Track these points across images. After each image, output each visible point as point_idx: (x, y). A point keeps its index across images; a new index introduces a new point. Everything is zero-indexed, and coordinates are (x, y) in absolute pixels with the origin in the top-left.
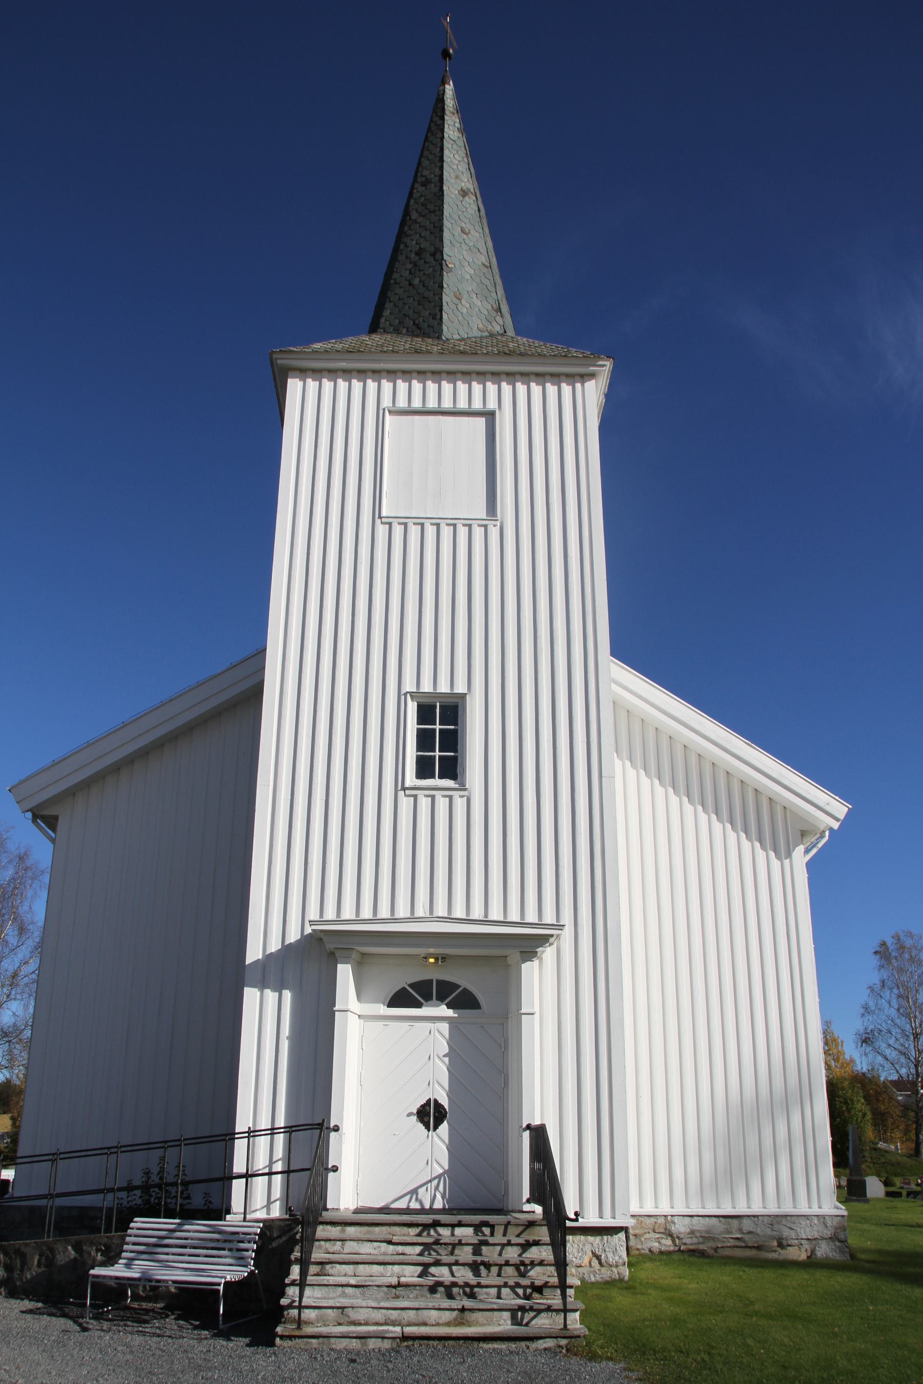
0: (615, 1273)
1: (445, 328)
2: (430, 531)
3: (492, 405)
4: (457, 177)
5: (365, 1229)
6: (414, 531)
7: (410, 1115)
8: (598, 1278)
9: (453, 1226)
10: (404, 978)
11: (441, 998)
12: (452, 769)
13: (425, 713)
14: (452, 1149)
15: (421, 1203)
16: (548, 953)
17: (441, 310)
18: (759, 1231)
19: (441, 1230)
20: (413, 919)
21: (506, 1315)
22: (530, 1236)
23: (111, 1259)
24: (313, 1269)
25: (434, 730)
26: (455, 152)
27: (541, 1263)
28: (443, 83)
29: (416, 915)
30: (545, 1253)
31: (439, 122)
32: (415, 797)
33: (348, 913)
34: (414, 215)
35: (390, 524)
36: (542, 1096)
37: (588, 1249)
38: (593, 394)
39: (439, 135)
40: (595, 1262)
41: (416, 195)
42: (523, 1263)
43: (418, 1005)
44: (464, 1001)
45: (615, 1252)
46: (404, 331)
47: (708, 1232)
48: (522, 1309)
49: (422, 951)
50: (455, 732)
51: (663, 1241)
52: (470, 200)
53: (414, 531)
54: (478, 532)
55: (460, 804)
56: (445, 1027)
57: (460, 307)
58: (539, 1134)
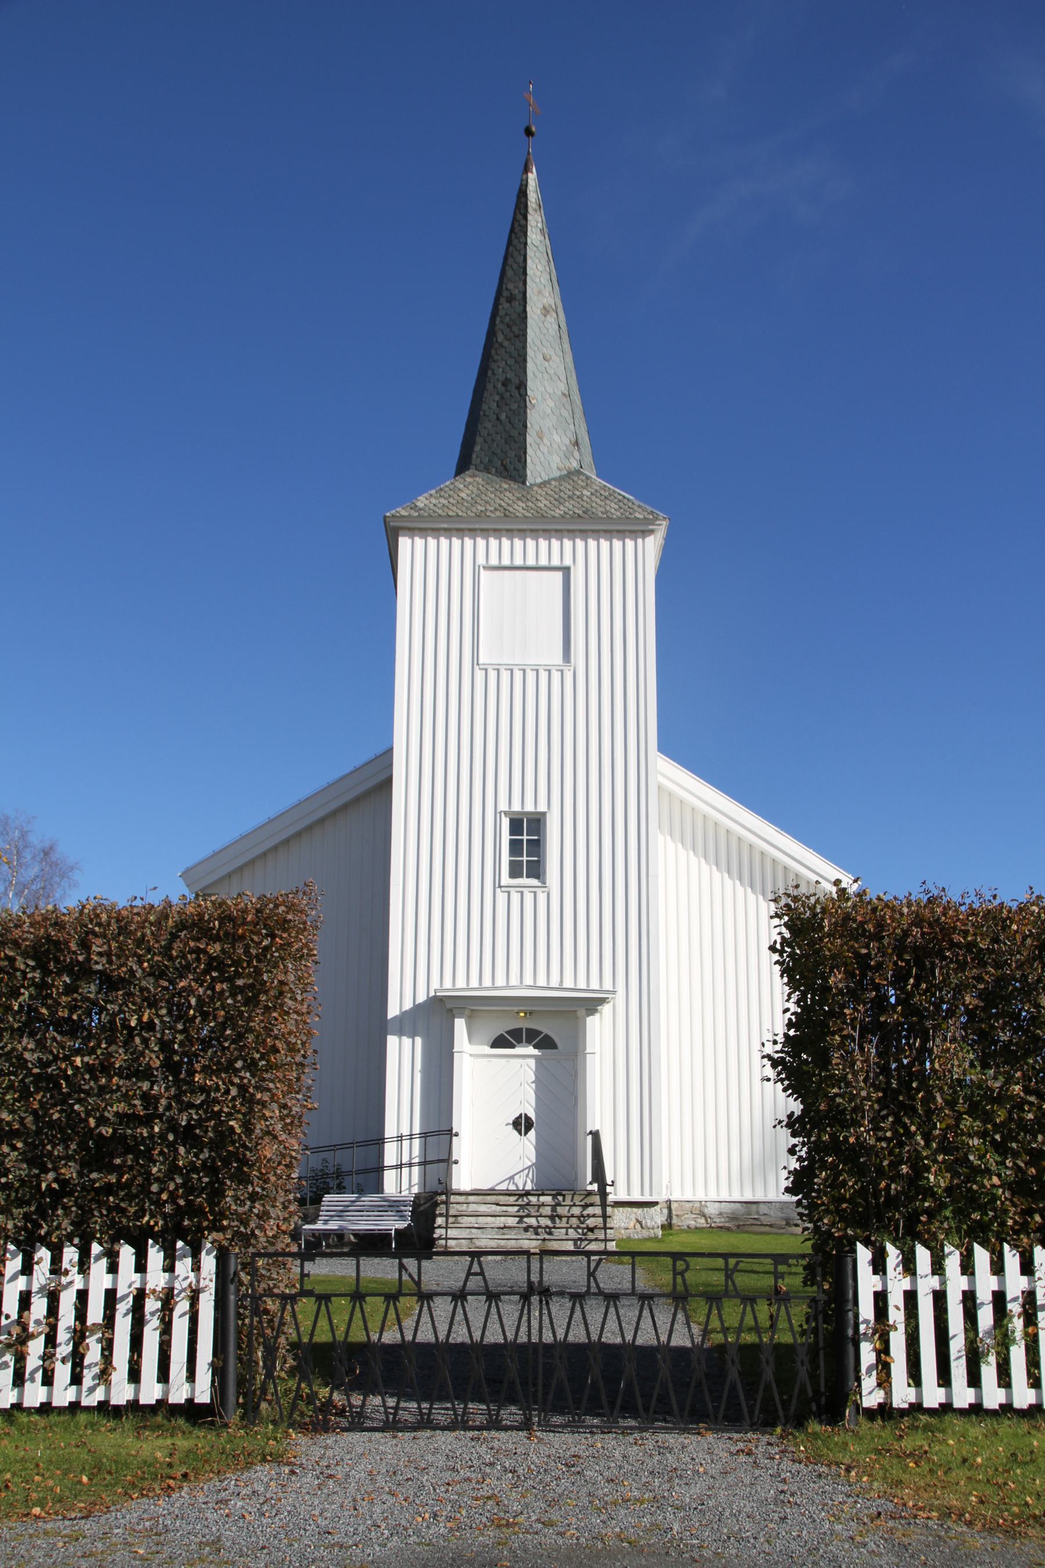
0: (652, 1233)
1: (529, 473)
2: (518, 675)
3: (568, 562)
4: (540, 292)
5: (481, 1197)
6: (505, 676)
7: (507, 1124)
8: (640, 1236)
9: (539, 1195)
10: (502, 1027)
11: (529, 1042)
12: (536, 870)
13: (516, 826)
14: (538, 1148)
15: (516, 1185)
16: (606, 1009)
17: (525, 453)
18: (772, 1213)
19: (531, 1198)
20: (508, 987)
21: (571, 1243)
22: (588, 1200)
23: (314, 1221)
24: (451, 1220)
25: (522, 840)
26: (537, 261)
27: (594, 1216)
28: (526, 170)
29: (511, 984)
30: (598, 1211)
31: (523, 222)
32: (509, 893)
33: (461, 983)
34: (500, 338)
35: (486, 670)
36: (601, 1109)
37: (633, 1217)
38: (651, 548)
39: (522, 240)
40: (638, 1226)
41: (501, 313)
42: (582, 1216)
43: (513, 1046)
44: (545, 1043)
45: (652, 1219)
46: (494, 470)
47: (732, 1213)
48: (580, 1239)
49: (516, 1009)
50: (538, 841)
51: (699, 1220)
52: (551, 319)
53: (505, 676)
54: (556, 676)
55: (542, 897)
56: (532, 1062)
57: (541, 446)
58: (596, 1135)
